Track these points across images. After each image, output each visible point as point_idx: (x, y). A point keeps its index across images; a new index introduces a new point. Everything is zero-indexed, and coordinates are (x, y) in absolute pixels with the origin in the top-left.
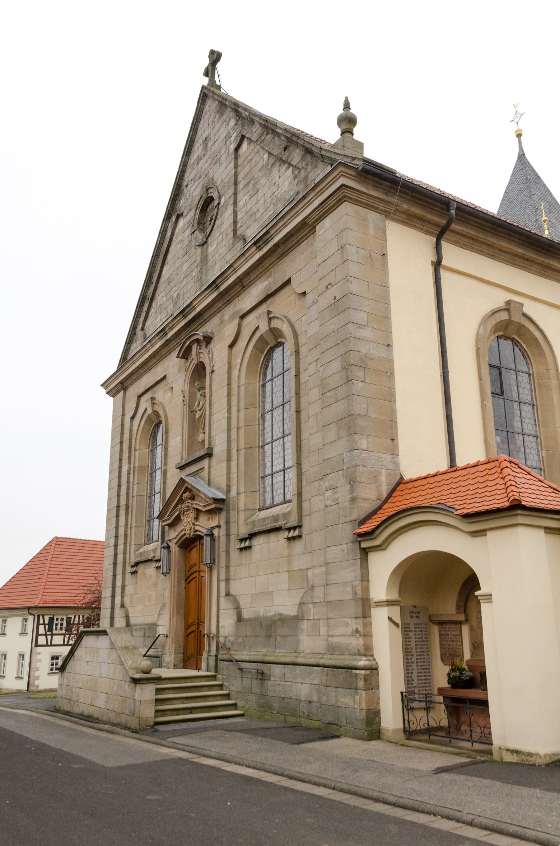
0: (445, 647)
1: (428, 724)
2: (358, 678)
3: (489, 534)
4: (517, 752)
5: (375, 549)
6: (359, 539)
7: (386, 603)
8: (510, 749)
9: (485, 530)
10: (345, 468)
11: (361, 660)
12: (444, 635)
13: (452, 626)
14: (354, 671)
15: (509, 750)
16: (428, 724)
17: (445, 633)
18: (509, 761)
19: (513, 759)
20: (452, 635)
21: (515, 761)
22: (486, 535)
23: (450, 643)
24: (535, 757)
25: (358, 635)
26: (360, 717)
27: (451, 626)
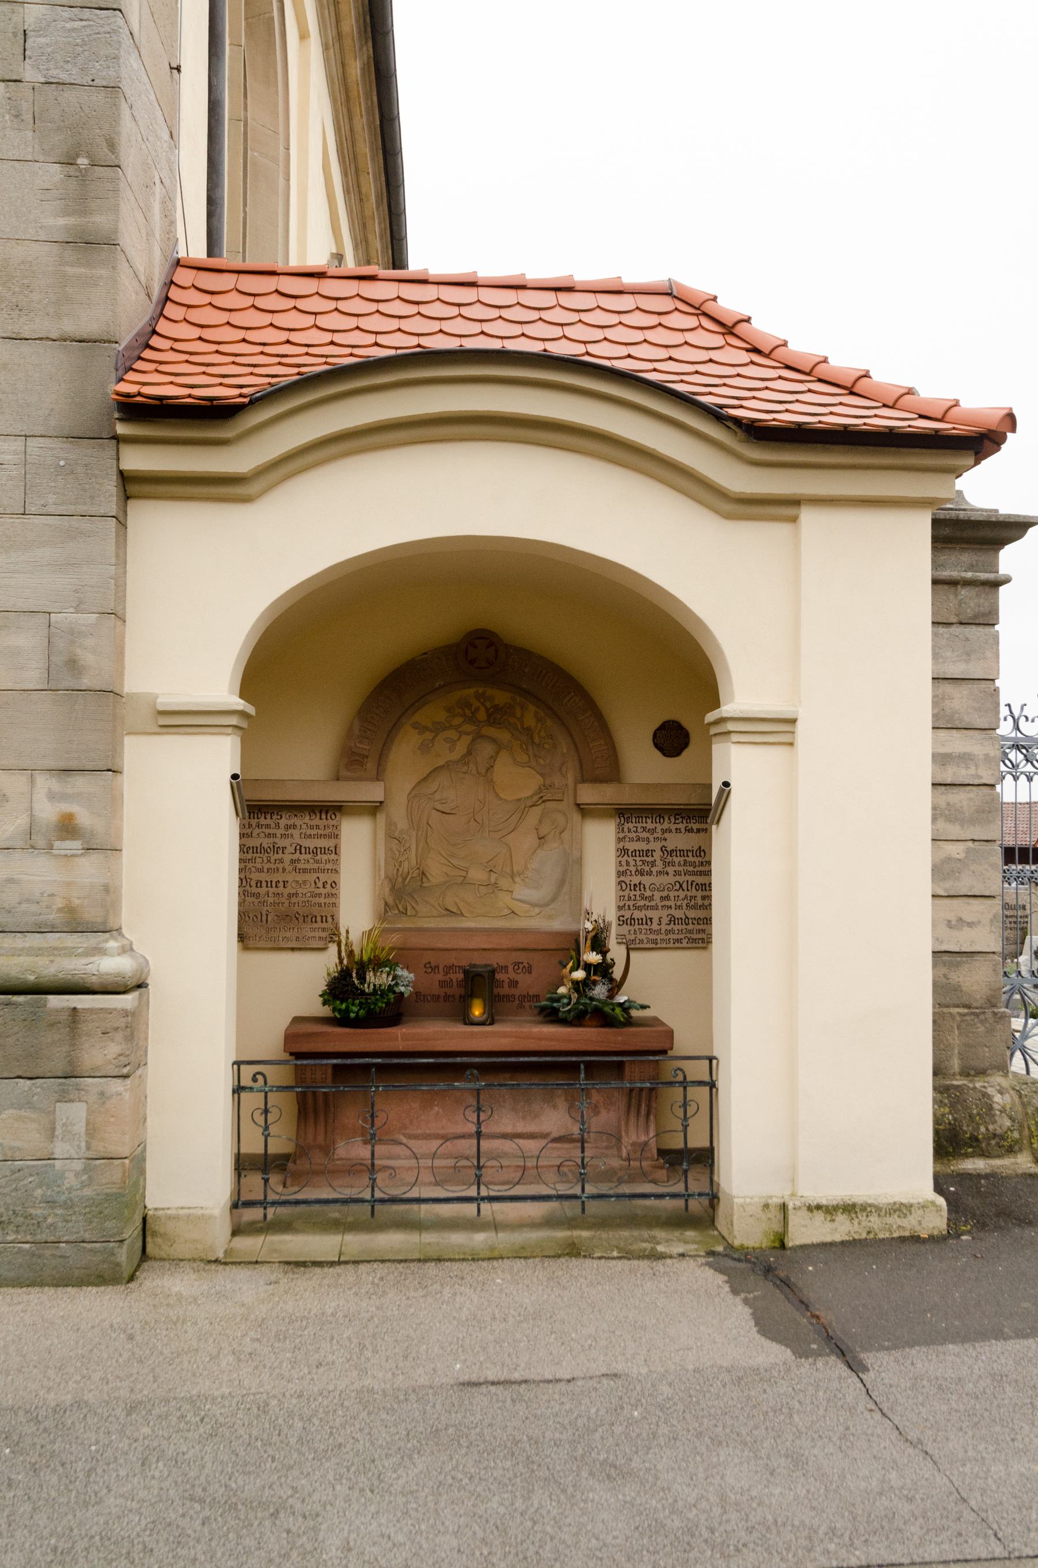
0: (263, 890)
1: (266, 1181)
2: (84, 1027)
3: (808, 516)
4: (850, 1209)
5: (162, 489)
6: (121, 429)
7: (234, 720)
8: (824, 1202)
9: (795, 502)
10: (31, 74)
11: (99, 951)
12: (259, 850)
13: (304, 820)
14: (55, 1001)
15: (819, 1207)
16: (266, 1181)
17: (266, 843)
18: (816, 1239)
19: (841, 1229)
20: (299, 849)
21: (838, 1238)
22: (794, 519)
23: (290, 877)
24: (920, 1212)
25: (76, 844)
26: (88, 1192)
27: (298, 822)
